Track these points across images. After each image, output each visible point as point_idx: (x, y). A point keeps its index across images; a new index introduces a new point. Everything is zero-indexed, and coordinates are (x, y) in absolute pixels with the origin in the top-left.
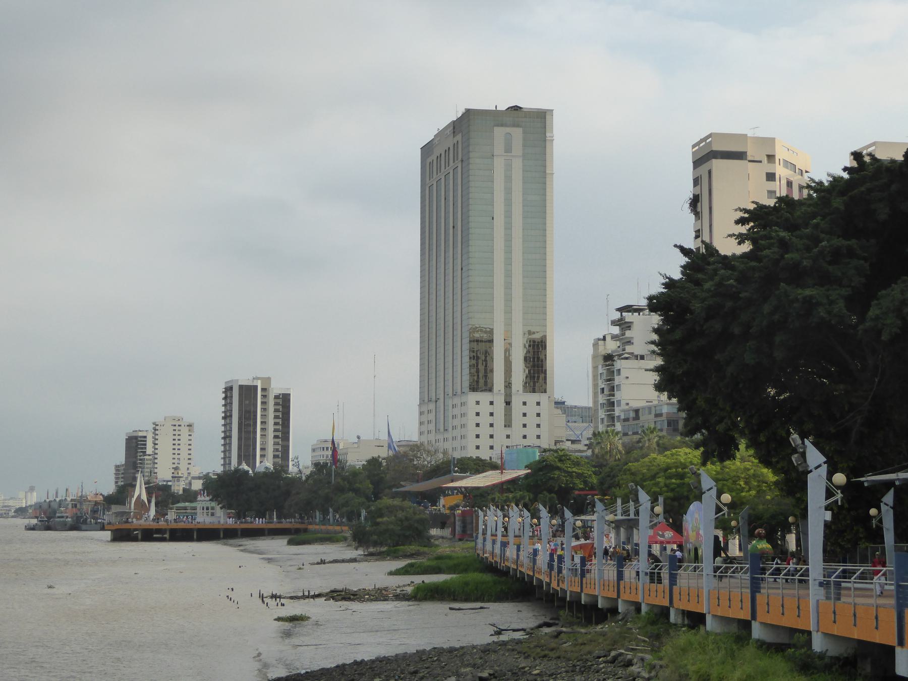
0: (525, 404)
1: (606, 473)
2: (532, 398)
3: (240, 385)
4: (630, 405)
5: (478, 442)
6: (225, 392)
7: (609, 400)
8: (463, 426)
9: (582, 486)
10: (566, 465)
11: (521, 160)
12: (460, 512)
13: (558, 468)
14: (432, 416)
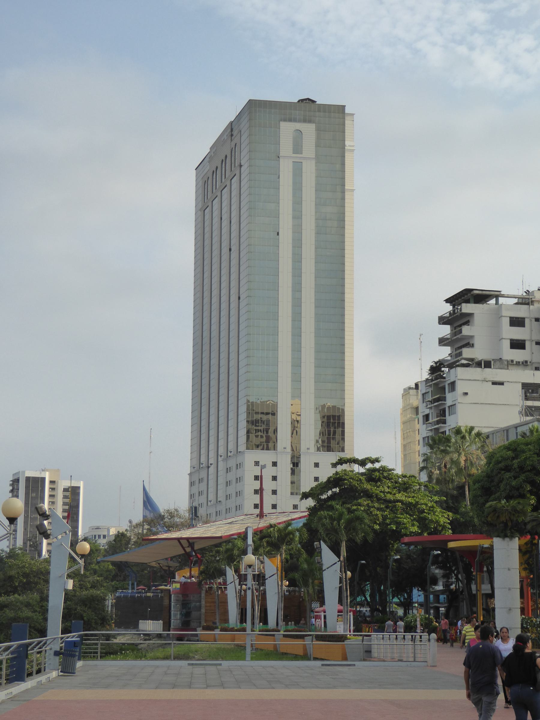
0: (317, 465)
1: (498, 462)
3: (26, 477)
6: (12, 485)
7: (437, 430)
8: (239, 494)
9: (415, 529)
10: (381, 488)
11: (313, 162)
12: (178, 586)
13: (368, 495)
14: (203, 487)
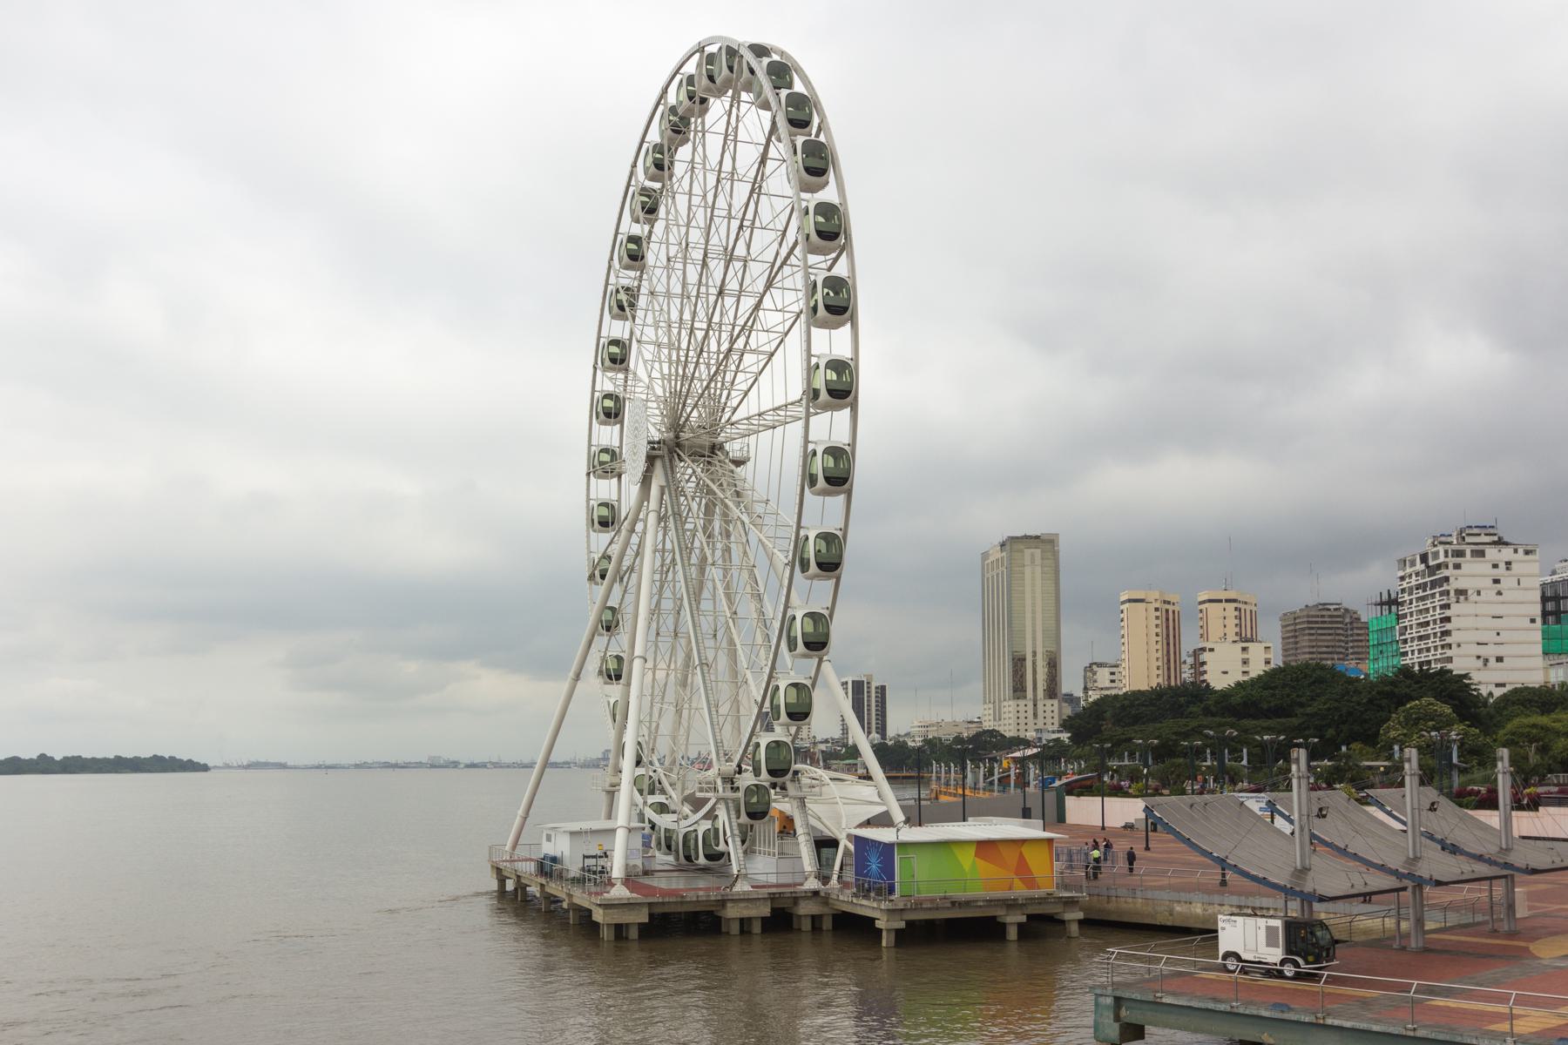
2: (1049, 702)
4: (1496, 550)
5: (1026, 709)
